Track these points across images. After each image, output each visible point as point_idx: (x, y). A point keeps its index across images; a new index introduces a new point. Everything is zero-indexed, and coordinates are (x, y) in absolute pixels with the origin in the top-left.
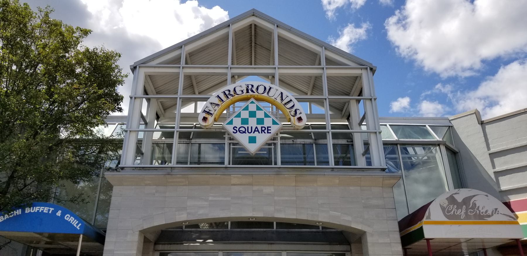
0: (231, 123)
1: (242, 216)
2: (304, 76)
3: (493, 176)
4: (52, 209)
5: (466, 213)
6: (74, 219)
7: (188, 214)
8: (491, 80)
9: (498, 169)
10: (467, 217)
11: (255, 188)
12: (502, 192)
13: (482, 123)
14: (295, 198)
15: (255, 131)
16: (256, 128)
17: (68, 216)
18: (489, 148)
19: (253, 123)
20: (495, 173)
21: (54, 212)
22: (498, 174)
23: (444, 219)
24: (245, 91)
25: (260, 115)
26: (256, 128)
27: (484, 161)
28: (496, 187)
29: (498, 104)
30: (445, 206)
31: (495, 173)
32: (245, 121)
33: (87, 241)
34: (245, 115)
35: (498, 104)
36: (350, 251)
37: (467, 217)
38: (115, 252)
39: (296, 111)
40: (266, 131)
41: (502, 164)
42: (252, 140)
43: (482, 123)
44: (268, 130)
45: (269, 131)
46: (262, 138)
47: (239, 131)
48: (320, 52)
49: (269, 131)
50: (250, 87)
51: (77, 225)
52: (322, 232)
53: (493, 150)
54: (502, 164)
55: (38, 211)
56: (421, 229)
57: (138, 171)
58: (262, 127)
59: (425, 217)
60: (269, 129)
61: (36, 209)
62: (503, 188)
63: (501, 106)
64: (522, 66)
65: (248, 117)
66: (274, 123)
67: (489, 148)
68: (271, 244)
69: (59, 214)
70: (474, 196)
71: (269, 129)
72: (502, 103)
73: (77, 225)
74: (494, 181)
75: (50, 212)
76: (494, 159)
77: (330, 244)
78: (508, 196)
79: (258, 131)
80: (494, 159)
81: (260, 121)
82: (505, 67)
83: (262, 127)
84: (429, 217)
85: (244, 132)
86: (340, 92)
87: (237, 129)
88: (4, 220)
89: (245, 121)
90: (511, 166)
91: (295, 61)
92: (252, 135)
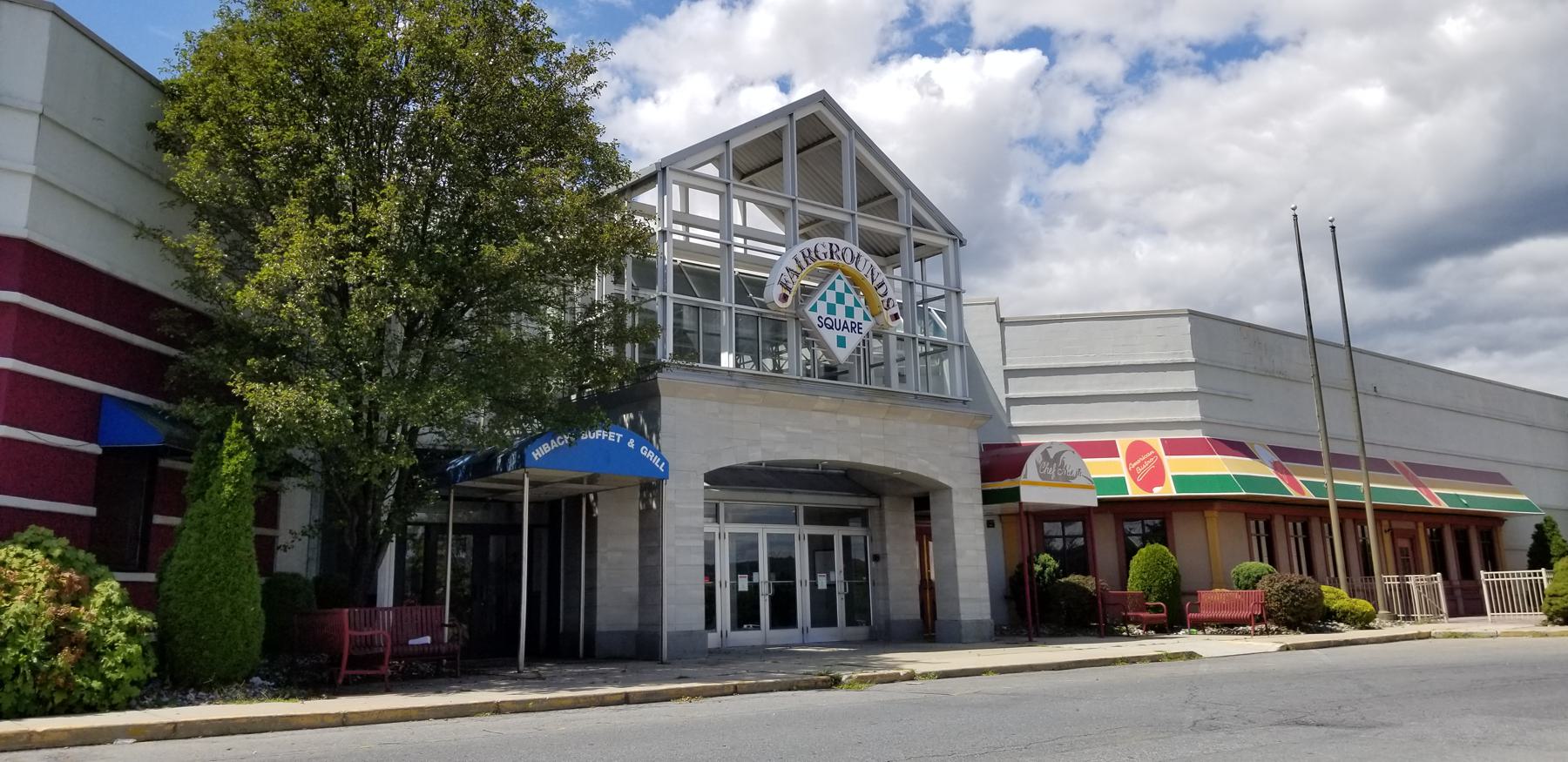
0: (814, 309)
1: (863, 462)
2: (869, 231)
3: (1004, 404)
4: (620, 436)
5: (1056, 473)
6: (653, 454)
7: (764, 451)
8: (652, 27)
9: (1011, 394)
10: (1057, 478)
11: (840, 417)
12: (1011, 427)
13: (1001, 321)
14: (882, 437)
15: (844, 327)
16: (845, 322)
17: (644, 450)
18: (1004, 364)
19: (840, 311)
20: (1008, 399)
21: (625, 440)
22: (1012, 402)
23: (1039, 480)
24: (829, 255)
25: (849, 300)
26: (845, 322)
27: (995, 378)
28: (1005, 420)
29: (652, 96)
30: (1040, 462)
31: (1008, 399)
32: (831, 309)
33: (1417, 560)
34: (831, 297)
35: (652, 96)
36: (881, 506)
37: (1057, 478)
38: (677, 506)
39: (888, 301)
40: (856, 329)
41: (1020, 388)
42: (841, 342)
43: (1001, 321)
44: (859, 328)
45: (860, 331)
46: (853, 340)
47: (826, 324)
48: (901, 196)
49: (860, 331)
50: (807, 254)
51: (660, 464)
52: (823, 474)
53: (1009, 366)
54: (1020, 388)
55: (600, 437)
56: (1017, 490)
57: (683, 372)
58: (852, 322)
59: (1022, 476)
60: (860, 326)
61: (599, 434)
62: (1015, 423)
63: (655, 102)
64: (725, 13)
65: (834, 302)
66: (866, 318)
67: (1004, 364)
68: (790, 493)
69: (631, 444)
70: (1063, 452)
71: (860, 326)
72: (662, 94)
73: (660, 464)
74: (1002, 407)
75: (618, 441)
76: (1009, 379)
77: (858, 496)
78: (1019, 436)
79: (847, 328)
80: (1009, 379)
81: (850, 312)
82: (692, 6)
83: (852, 322)
84: (1025, 477)
85: (831, 328)
86: (867, 246)
87: (823, 321)
88: (551, 451)
89: (831, 309)
90: (1029, 393)
91: (827, 181)
92: (840, 333)
